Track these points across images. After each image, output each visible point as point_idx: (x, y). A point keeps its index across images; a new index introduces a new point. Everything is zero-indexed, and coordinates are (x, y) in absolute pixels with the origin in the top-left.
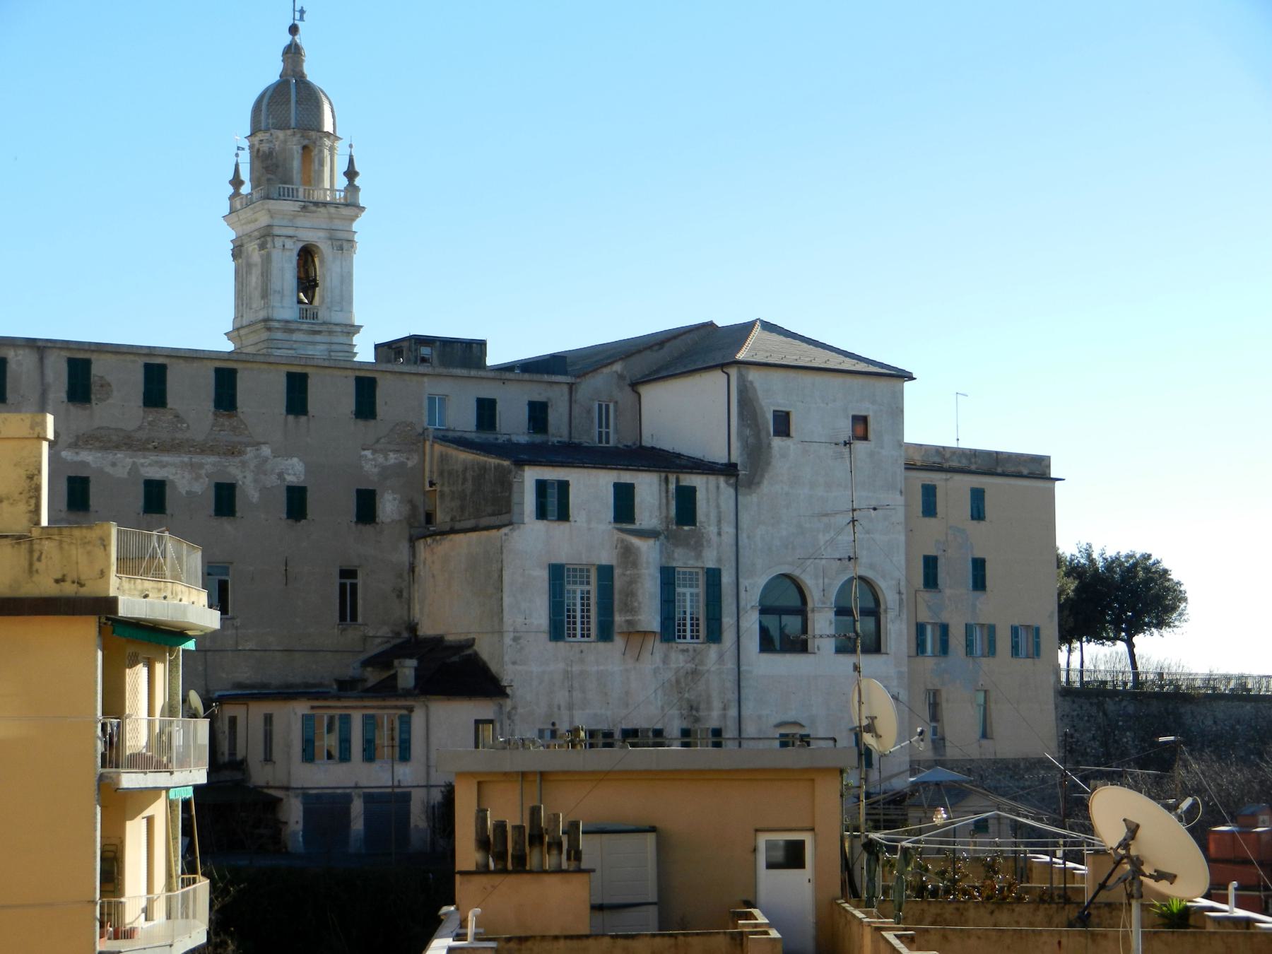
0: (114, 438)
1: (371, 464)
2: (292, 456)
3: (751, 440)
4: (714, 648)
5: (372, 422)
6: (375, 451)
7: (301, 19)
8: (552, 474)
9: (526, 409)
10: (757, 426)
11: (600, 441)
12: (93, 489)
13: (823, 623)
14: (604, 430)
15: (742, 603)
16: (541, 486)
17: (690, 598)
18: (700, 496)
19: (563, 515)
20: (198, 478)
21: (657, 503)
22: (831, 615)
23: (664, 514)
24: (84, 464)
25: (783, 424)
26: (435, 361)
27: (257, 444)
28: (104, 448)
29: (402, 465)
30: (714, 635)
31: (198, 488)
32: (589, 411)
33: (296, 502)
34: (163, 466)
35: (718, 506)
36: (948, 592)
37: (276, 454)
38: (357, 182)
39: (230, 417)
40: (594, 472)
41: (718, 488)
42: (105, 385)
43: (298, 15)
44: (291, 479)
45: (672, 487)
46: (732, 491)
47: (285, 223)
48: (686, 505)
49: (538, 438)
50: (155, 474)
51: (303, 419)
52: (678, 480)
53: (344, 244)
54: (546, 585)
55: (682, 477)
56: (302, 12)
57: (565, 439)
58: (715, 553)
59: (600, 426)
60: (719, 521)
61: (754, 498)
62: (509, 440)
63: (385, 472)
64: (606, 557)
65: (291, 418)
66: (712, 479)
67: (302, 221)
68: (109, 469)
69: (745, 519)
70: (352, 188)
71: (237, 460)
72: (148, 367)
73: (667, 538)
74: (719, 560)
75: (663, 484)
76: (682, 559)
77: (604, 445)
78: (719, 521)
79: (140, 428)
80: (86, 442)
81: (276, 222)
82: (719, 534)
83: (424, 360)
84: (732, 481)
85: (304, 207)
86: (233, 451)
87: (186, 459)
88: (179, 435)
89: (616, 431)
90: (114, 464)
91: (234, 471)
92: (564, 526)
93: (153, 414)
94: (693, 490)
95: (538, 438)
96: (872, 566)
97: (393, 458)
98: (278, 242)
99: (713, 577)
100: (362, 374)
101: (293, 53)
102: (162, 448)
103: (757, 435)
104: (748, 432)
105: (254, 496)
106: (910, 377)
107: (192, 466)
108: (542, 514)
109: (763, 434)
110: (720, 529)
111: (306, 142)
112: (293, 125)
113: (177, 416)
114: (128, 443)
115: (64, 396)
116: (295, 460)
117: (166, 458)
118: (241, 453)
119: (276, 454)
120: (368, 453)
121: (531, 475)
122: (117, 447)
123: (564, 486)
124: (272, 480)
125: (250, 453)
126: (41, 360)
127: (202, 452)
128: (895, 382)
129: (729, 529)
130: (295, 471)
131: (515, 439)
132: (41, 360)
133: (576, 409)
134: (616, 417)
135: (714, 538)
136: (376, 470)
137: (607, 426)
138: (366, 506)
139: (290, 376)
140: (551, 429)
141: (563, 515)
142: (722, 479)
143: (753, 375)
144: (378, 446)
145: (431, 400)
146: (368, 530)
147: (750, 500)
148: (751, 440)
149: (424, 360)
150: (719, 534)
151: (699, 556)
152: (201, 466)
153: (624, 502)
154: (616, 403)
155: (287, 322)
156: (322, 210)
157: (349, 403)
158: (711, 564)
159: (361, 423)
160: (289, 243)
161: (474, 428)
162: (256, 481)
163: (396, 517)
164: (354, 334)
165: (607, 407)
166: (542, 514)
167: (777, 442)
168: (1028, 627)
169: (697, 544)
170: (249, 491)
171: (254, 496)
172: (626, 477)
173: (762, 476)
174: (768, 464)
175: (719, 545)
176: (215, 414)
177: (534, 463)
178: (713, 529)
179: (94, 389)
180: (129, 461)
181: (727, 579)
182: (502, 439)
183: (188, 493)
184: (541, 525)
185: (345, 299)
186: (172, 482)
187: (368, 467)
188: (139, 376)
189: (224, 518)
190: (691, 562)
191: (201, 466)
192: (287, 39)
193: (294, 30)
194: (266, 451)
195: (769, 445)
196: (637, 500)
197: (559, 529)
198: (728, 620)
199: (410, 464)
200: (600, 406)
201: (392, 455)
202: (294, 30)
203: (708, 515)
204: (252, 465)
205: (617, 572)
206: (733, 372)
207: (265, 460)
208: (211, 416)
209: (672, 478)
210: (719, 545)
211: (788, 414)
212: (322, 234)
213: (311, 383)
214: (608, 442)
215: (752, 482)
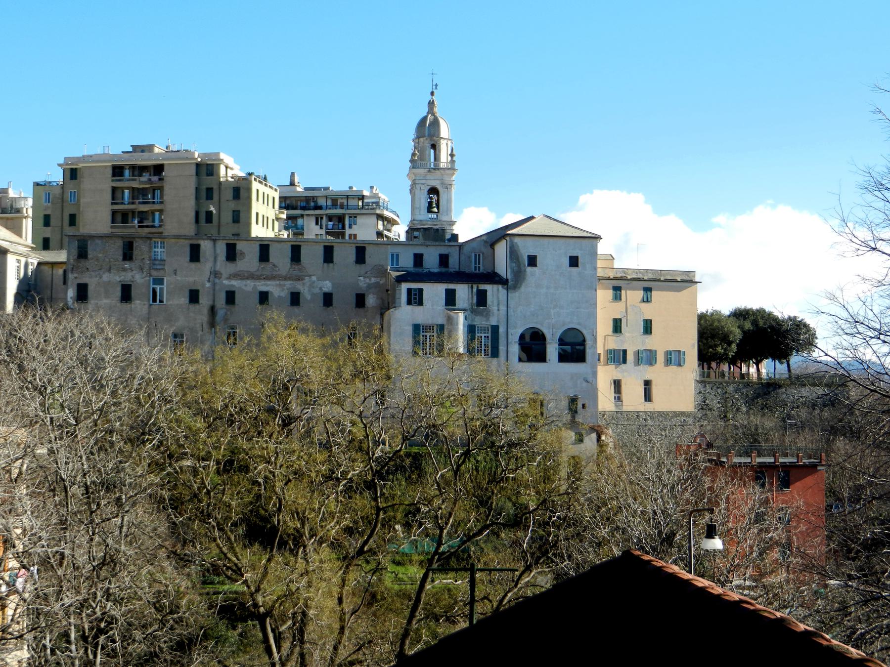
0: (246, 275)
1: (363, 283)
2: (326, 280)
3: (516, 269)
4: (495, 361)
5: (363, 265)
6: (365, 277)
7: (436, 88)
8: (414, 286)
9: (438, 257)
10: (519, 262)
11: (475, 270)
12: (237, 296)
13: (552, 350)
14: (477, 265)
15: (510, 341)
16: (409, 291)
17: (482, 336)
18: (489, 294)
19: (420, 303)
20: (283, 290)
21: (467, 298)
22: (557, 346)
23: (471, 301)
24: (233, 286)
25: (532, 261)
26: (421, 237)
27: (310, 276)
28: (242, 279)
29: (378, 283)
30: (495, 354)
31: (283, 294)
32: (469, 257)
33: (328, 299)
34: (267, 285)
35: (498, 298)
36: (627, 335)
37: (318, 279)
38: (455, 159)
39: (297, 265)
40: (436, 284)
41: (498, 290)
42: (242, 253)
43: (434, 87)
44: (325, 290)
45: (475, 290)
46: (505, 291)
47: (422, 178)
48: (482, 299)
49: (444, 270)
50: (264, 289)
51: (331, 265)
52: (478, 287)
53: (448, 186)
54: (411, 333)
55: (480, 285)
56: (436, 85)
57: (457, 269)
58: (496, 318)
59: (475, 264)
60: (498, 304)
61: (517, 294)
62: (429, 271)
63: (369, 286)
64: (440, 320)
65: (326, 265)
66: (495, 286)
67: (429, 177)
68: (244, 287)
69: (512, 304)
70: (453, 162)
71: (301, 282)
72: (261, 246)
73: (472, 312)
74: (498, 321)
75: (470, 289)
76: (478, 321)
77: (477, 272)
78: (498, 304)
79: (258, 270)
80: (234, 277)
81: (417, 178)
82: (498, 310)
83: (415, 237)
84: (506, 287)
85: (429, 171)
86: (299, 279)
87: (278, 283)
88: (275, 273)
89: (483, 266)
90: (246, 285)
91: (299, 287)
92: (420, 308)
93: (263, 265)
94: (485, 291)
95: (444, 270)
96: (579, 324)
97: (373, 280)
98: (418, 186)
99: (495, 329)
100: (359, 245)
101: (431, 104)
102: (267, 278)
103: (519, 266)
104: (514, 265)
105: (309, 297)
106: (599, 238)
107: (280, 285)
108: (409, 302)
109: (522, 265)
110: (498, 308)
111: (433, 142)
112: (427, 134)
113: (274, 265)
114: (252, 276)
115: (224, 258)
116: (327, 282)
117: (269, 283)
118: (303, 279)
119: (318, 279)
120: (361, 278)
121: (405, 286)
122: (247, 278)
123: (421, 291)
124: (317, 291)
125: (307, 279)
126: (215, 244)
127: (285, 279)
128: (594, 240)
129: (503, 308)
130: (327, 286)
131: (432, 270)
132: (215, 244)
133: (463, 258)
134: (483, 259)
135: (496, 311)
136: (365, 285)
137: (479, 264)
138: (360, 300)
139: (325, 247)
140: (450, 266)
141: (420, 303)
142: (500, 286)
143: (517, 240)
144: (367, 275)
145: (392, 255)
146: (361, 310)
147: (514, 296)
148: (516, 269)
149: (415, 237)
150: (498, 310)
151: (488, 320)
152: (284, 285)
153: (450, 298)
154: (483, 253)
155: (421, 221)
156: (437, 171)
157: (353, 257)
158: (494, 323)
159: (358, 266)
160: (423, 187)
161: (412, 266)
162: (309, 291)
163: (374, 305)
164: (453, 225)
165: (479, 255)
166: (409, 302)
167: (529, 269)
168: (675, 351)
169: (487, 315)
170: (306, 294)
171: (309, 297)
172: (451, 286)
173: (521, 284)
174: (524, 279)
175: (498, 315)
176: (291, 264)
177: (406, 281)
178: (495, 308)
179: (238, 255)
180: (252, 284)
181: (502, 330)
182: (425, 271)
183: (279, 296)
184: (410, 307)
185: (449, 211)
186: (272, 292)
187: (361, 284)
188: (257, 249)
189: (295, 307)
190: (484, 323)
191: (284, 285)
192: (429, 97)
193: (432, 94)
194: (314, 278)
195: (525, 271)
196: (457, 296)
197: (417, 309)
198: (502, 348)
199: (381, 282)
200: (476, 255)
201: (373, 279)
202: (432, 94)
203: (493, 302)
204: (308, 284)
205: (446, 327)
206: (508, 238)
207: (314, 282)
208: (289, 265)
209: (475, 287)
210: (498, 315)
211: (577, 257)
212: (438, 182)
213: (335, 249)
214: (479, 270)
215: (516, 287)
